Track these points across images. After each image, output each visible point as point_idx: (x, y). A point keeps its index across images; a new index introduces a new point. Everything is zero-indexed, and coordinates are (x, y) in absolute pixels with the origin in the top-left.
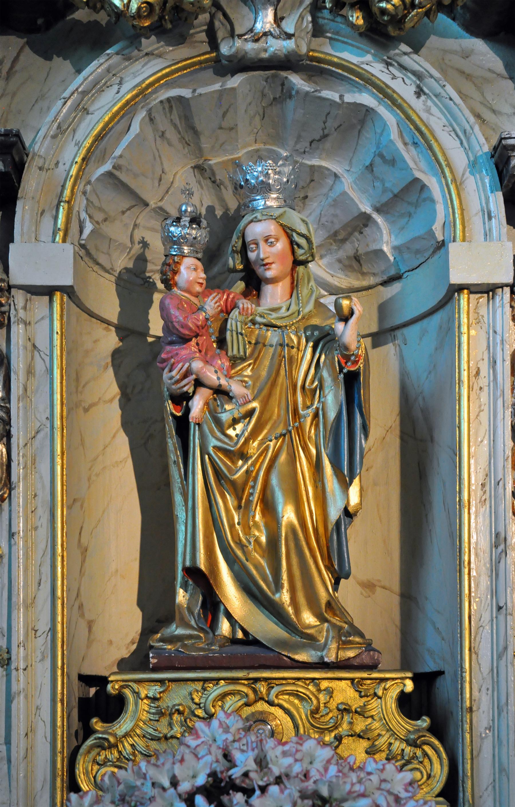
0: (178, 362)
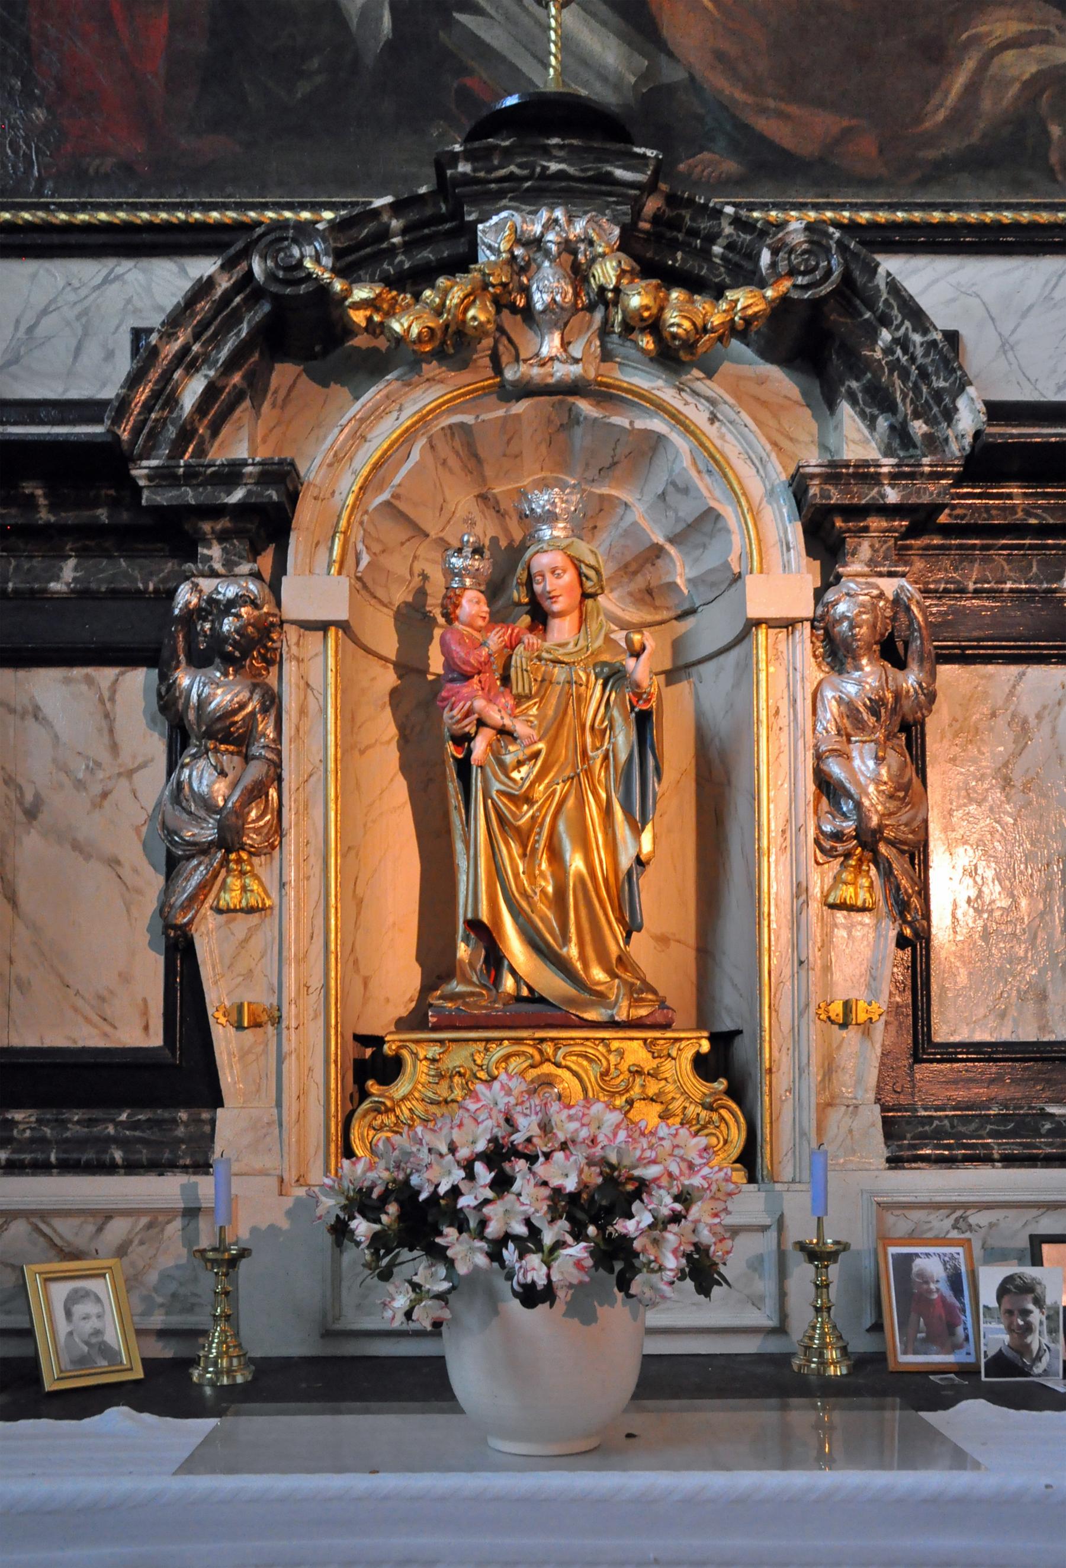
0: (460, 701)
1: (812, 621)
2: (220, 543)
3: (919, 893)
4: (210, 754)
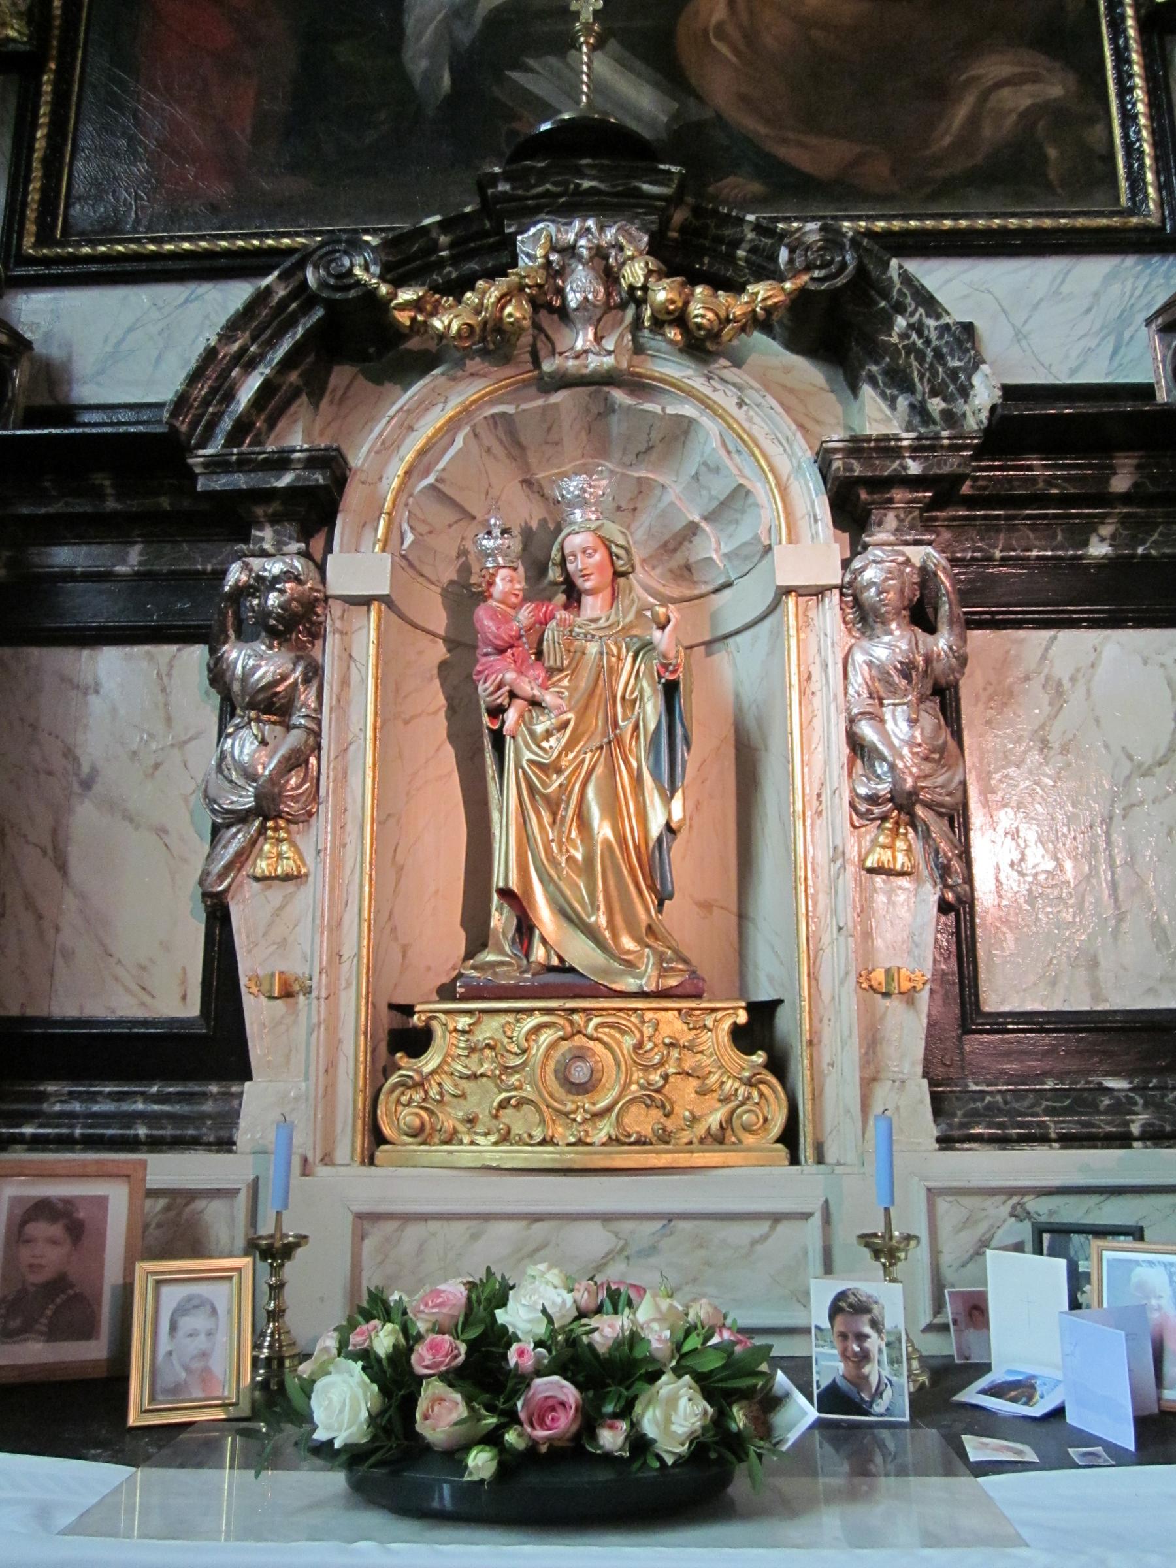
1: (841, 588)
2: (272, 526)
3: (960, 856)
4: (253, 724)
